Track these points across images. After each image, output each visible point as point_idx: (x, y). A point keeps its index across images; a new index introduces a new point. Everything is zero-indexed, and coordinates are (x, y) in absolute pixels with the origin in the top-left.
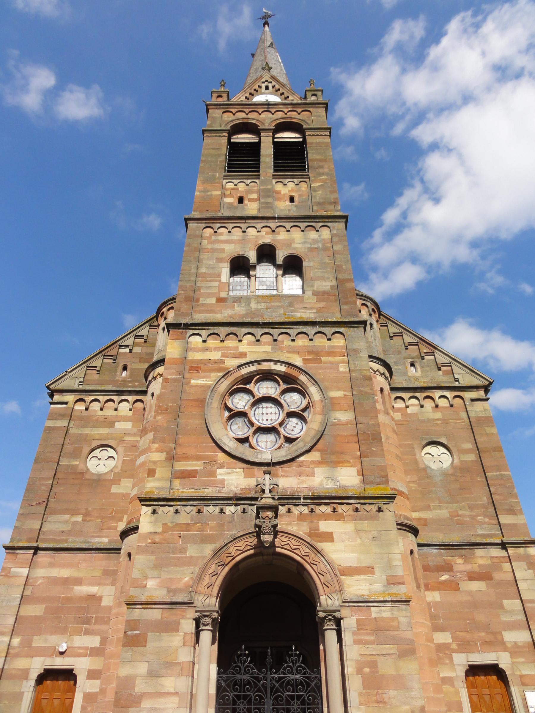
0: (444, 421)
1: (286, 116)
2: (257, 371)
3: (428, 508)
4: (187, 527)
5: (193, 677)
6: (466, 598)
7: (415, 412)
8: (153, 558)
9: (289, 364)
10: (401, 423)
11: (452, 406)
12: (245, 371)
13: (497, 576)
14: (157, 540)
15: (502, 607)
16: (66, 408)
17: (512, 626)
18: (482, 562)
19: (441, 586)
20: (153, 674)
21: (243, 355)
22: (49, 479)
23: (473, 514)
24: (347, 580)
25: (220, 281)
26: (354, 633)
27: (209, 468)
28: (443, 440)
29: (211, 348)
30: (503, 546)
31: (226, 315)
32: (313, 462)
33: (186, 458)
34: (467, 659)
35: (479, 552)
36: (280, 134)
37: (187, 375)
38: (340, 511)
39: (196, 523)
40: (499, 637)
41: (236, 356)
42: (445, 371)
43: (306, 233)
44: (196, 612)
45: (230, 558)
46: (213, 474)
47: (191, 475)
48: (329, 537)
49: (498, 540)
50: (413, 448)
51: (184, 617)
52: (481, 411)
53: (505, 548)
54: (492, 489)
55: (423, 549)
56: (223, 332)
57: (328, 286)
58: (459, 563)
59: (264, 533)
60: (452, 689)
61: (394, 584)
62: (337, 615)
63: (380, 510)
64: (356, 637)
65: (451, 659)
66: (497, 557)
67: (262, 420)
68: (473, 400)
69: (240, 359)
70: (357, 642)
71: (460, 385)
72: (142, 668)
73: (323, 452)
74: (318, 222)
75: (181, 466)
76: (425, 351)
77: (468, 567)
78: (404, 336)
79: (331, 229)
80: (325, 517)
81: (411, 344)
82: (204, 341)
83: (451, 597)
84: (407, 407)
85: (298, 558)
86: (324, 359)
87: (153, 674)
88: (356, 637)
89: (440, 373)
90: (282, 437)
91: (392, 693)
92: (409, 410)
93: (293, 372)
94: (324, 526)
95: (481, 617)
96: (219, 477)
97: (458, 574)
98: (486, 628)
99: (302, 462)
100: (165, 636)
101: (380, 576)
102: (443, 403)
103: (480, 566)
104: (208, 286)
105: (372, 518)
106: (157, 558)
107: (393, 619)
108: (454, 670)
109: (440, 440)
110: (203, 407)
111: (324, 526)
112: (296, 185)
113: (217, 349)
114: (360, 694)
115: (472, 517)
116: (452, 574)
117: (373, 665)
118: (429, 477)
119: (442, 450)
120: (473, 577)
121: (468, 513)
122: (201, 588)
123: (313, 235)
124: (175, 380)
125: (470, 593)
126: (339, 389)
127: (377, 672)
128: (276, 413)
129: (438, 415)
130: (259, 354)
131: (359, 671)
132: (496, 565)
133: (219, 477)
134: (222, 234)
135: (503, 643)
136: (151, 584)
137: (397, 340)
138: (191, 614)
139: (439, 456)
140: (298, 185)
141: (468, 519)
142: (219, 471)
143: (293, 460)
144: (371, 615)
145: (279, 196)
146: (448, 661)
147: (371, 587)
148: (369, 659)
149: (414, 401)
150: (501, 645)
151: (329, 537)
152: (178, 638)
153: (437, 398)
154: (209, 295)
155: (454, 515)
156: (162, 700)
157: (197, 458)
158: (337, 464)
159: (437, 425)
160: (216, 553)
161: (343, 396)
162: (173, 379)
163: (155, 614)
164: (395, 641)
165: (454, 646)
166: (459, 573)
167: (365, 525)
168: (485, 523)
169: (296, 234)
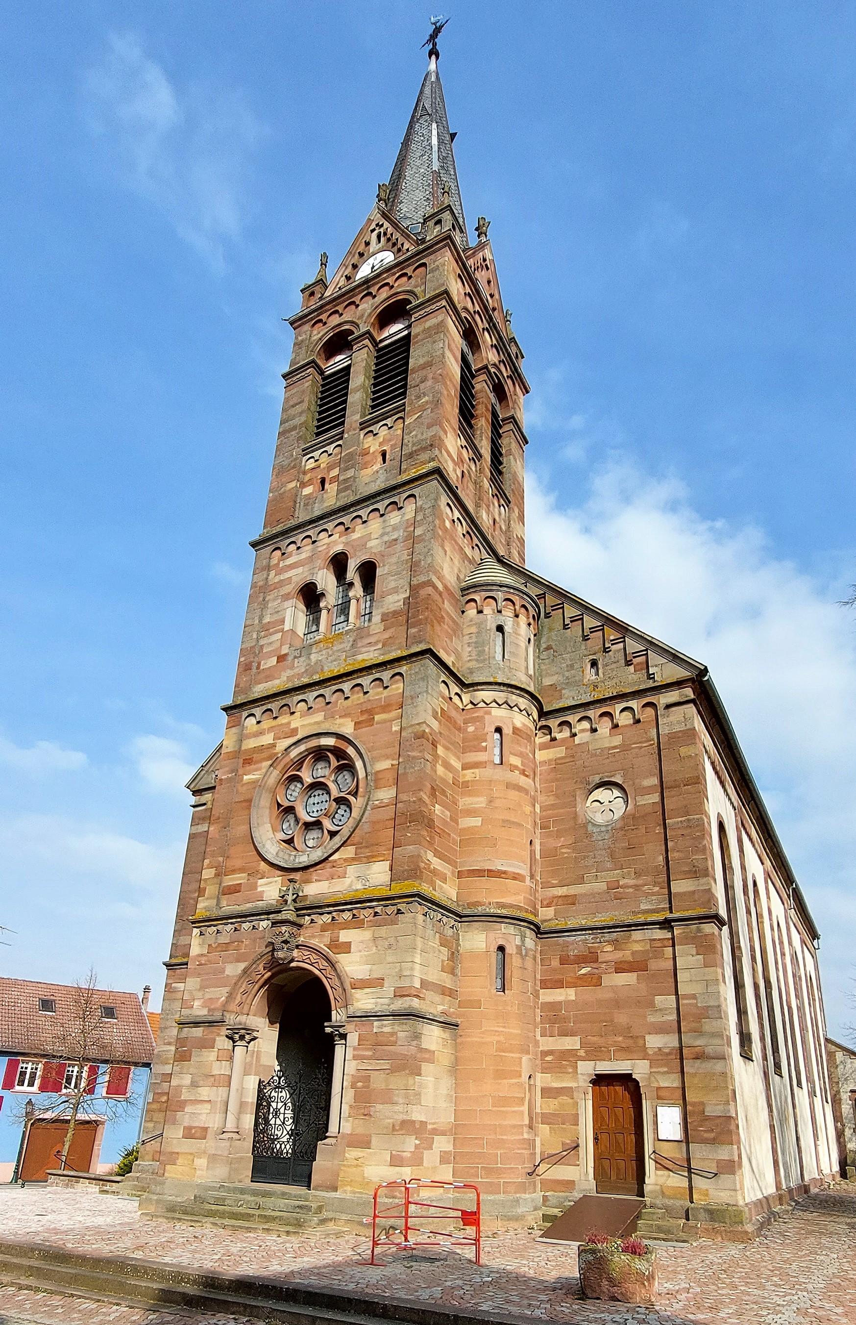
0: (624, 748)
1: (393, 291)
2: (306, 750)
3: (581, 880)
4: (225, 947)
5: (229, 1086)
6: (609, 995)
7: (585, 741)
8: (199, 979)
9: (339, 736)
10: (563, 761)
11: (638, 721)
12: (294, 753)
13: (653, 965)
14: (203, 962)
15: (652, 1004)
16: (206, 809)
17: (660, 1029)
18: (637, 947)
19: (578, 982)
20: (194, 1085)
21: (294, 731)
22: (195, 892)
23: (640, 882)
24: (358, 994)
25: (282, 630)
26: (355, 1049)
27: (252, 880)
28: (618, 779)
29: (265, 729)
30: (666, 924)
31: (285, 679)
32: (345, 860)
33: (233, 871)
34: (595, 1068)
35: (637, 935)
36: (387, 331)
37: (240, 772)
38: (341, 920)
39: (233, 942)
40: (641, 1042)
41: (289, 735)
42: (638, 664)
43: (386, 517)
44: (227, 1029)
45: (260, 976)
46: (255, 886)
47: (235, 889)
48: (346, 948)
49: (660, 917)
50: (575, 796)
51: (219, 1035)
52: (679, 722)
53: (671, 929)
54: (670, 844)
55: (563, 936)
56: (274, 706)
57: (399, 601)
58: (608, 953)
59: (278, 950)
60: (571, 1101)
61: (401, 996)
62: (341, 1030)
63: (399, 912)
64: (356, 1053)
65: (576, 1067)
66: (659, 940)
67: (313, 812)
68: (668, 706)
69: (291, 738)
70: (355, 1058)
71: (656, 684)
72: (187, 1080)
73: (358, 846)
74: (399, 493)
75: (230, 880)
76: (612, 638)
77: (618, 955)
78: (585, 617)
79: (417, 499)
80: (346, 926)
81: (593, 630)
82: (258, 722)
83: (590, 994)
84: (575, 735)
85: (317, 972)
86: (377, 718)
87: (194, 1085)
88: (356, 1053)
89: (632, 668)
90: (326, 832)
91: (379, 1107)
92: (577, 740)
93: (342, 745)
94: (345, 936)
95: (622, 1018)
96: (259, 889)
97: (603, 966)
98: (626, 1031)
99: (335, 861)
100: (205, 1052)
101: (389, 990)
102: (624, 719)
103: (633, 953)
104: (270, 641)
105: (394, 923)
106: (202, 980)
107: (393, 1034)
108: (576, 1080)
109: (613, 779)
110: (249, 808)
111: (345, 936)
112: (390, 428)
113: (271, 729)
114: (351, 1106)
115: (637, 887)
116: (595, 965)
117: (367, 1079)
118: (589, 835)
119: (617, 793)
120: (620, 968)
121: (631, 882)
122: (233, 1007)
123: (394, 518)
124: (229, 780)
125: (614, 988)
126: (387, 757)
127: (368, 1087)
128: (326, 801)
129: (617, 740)
130: (310, 727)
131: (353, 1086)
132: (656, 950)
133: (259, 889)
134: (290, 555)
135: (644, 1048)
136: (197, 1004)
137: (576, 628)
138: (224, 1032)
139: (610, 802)
140: (392, 427)
141: (631, 890)
142: (260, 882)
143: (327, 858)
144: (373, 1030)
145: (367, 458)
146: (571, 1070)
147: (378, 1000)
148: (363, 1073)
149: (586, 725)
150: (643, 1053)
151: (346, 948)
152: (213, 1053)
153: (617, 713)
154: (269, 655)
155: (613, 886)
156: (199, 1106)
157: (242, 870)
158: (370, 859)
159: (614, 755)
160: (245, 971)
161: (390, 766)
162: (226, 779)
163: (198, 1032)
164: (391, 1057)
165: (582, 1053)
166: (605, 964)
167: (383, 931)
168: (653, 894)
169: (375, 525)
